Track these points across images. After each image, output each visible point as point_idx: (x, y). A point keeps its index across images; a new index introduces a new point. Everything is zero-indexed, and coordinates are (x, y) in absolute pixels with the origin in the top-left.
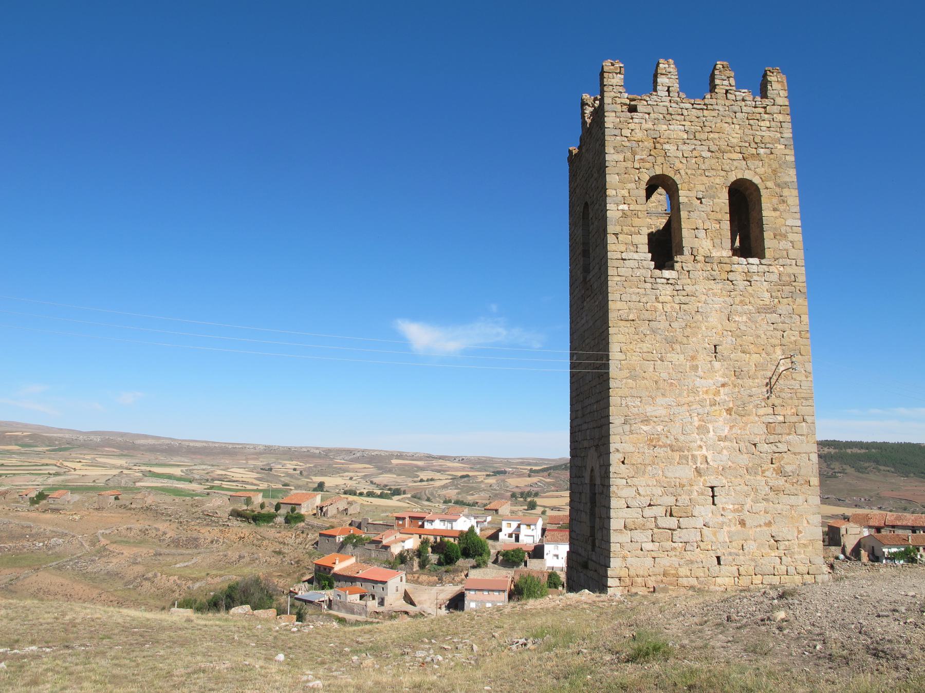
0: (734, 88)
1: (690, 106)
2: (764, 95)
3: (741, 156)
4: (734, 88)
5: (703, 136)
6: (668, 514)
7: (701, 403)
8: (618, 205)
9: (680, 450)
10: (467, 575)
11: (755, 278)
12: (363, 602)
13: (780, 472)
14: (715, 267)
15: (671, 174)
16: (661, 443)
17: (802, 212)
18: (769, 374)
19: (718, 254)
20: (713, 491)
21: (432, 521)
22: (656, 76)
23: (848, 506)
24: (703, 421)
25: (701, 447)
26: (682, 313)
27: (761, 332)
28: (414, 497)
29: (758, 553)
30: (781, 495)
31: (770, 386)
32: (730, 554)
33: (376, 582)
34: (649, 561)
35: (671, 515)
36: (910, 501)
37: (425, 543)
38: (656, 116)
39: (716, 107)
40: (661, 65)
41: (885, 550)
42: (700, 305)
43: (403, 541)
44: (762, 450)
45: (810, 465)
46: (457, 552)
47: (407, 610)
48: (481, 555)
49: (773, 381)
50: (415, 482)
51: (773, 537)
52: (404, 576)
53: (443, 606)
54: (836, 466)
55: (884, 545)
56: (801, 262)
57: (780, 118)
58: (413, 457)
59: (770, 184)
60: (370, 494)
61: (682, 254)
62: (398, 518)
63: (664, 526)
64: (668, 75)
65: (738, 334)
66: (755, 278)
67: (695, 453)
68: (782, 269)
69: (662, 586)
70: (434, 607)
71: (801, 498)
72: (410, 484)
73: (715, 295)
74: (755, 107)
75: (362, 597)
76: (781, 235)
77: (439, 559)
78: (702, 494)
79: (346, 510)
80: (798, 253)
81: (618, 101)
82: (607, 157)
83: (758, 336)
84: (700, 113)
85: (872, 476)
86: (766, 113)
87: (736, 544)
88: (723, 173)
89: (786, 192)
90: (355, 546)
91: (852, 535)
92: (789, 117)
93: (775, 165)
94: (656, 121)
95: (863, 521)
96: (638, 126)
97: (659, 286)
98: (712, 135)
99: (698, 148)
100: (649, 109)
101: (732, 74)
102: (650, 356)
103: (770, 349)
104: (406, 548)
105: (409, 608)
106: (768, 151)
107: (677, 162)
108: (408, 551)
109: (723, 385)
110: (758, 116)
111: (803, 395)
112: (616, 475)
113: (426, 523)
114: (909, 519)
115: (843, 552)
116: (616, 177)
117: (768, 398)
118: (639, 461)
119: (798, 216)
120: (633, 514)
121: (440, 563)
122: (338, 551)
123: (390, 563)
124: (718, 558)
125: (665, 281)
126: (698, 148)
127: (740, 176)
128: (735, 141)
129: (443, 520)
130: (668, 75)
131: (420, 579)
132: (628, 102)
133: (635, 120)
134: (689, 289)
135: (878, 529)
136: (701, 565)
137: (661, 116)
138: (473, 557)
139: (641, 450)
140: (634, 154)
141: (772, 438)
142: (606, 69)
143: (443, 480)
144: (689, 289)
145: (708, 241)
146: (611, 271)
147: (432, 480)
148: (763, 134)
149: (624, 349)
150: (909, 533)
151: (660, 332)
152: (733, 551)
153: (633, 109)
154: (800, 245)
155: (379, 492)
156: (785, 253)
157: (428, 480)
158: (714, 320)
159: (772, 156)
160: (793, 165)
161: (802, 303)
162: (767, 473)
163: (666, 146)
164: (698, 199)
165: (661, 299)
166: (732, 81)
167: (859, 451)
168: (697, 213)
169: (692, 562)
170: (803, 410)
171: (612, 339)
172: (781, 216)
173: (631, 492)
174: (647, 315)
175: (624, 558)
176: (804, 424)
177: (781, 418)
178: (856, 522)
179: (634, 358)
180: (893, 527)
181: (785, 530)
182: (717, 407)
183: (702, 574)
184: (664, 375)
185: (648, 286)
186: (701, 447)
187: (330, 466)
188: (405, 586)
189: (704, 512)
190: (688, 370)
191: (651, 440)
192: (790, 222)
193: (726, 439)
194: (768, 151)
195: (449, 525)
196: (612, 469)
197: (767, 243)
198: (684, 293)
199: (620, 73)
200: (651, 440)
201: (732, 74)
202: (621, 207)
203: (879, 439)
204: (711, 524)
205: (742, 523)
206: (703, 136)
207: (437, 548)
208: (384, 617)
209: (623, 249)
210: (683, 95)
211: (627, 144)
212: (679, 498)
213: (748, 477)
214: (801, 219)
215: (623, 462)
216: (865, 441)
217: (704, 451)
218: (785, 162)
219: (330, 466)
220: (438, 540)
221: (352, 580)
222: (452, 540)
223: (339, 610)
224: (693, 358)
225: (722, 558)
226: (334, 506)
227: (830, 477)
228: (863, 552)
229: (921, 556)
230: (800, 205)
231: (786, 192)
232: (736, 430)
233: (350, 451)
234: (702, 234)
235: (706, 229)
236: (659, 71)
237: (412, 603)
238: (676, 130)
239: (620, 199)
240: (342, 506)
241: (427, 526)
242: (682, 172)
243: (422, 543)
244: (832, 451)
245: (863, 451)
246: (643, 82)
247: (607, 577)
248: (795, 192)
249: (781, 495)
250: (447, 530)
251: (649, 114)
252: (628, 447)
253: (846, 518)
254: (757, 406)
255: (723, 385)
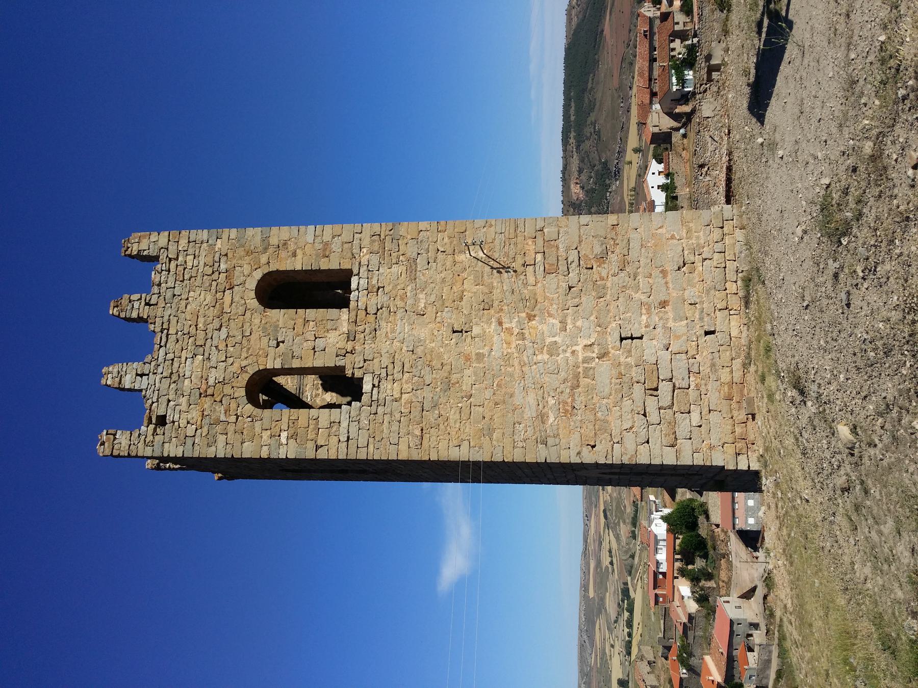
0: (144, 295)
1: (162, 351)
2: (155, 259)
3: (228, 292)
4: (144, 295)
5: (201, 335)
6: (655, 393)
7: (521, 350)
8: (281, 444)
9: (577, 376)
10: (718, 526)
11: (374, 282)
12: (756, 649)
13: (602, 258)
14: (361, 328)
15: (246, 377)
16: (570, 400)
17: (298, 223)
18: (488, 269)
19: (345, 324)
20: (626, 338)
21: (658, 564)
22: (124, 389)
23: (628, 119)
24: (542, 349)
25: (573, 352)
26: (414, 370)
27: (438, 278)
28: (630, 574)
29: (700, 286)
30: (629, 258)
31: (502, 269)
32: (701, 319)
33: (732, 632)
34: (713, 417)
35: (656, 389)
36: (623, 60)
37: (683, 573)
38: (172, 392)
39: (166, 318)
40: (109, 383)
41: (675, 88)
42: (405, 349)
43: (683, 597)
44: (577, 279)
45: (592, 225)
46: (691, 537)
47: (762, 596)
48: (693, 509)
49: (496, 265)
50: (613, 571)
51: (679, 269)
52: (723, 599)
53: (755, 554)
54: (588, 130)
55: (670, 89)
56: (358, 227)
57: (183, 243)
58: (586, 573)
59: (264, 259)
60: (629, 624)
61: (343, 368)
62: (657, 602)
63: (670, 398)
64: (122, 374)
65: (440, 304)
66: (374, 282)
67: (580, 359)
68: (365, 250)
69: (745, 405)
70: (755, 566)
71: (633, 235)
72: (616, 576)
73: (393, 331)
74: (169, 271)
75: (751, 650)
76: (325, 250)
77: (701, 557)
78: (630, 351)
79: (649, 663)
80: (347, 230)
81: (150, 438)
82: (221, 455)
83: (443, 280)
84: (172, 338)
85: (599, 95)
86: (177, 259)
87: (688, 311)
88: (248, 314)
89: (274, 241)
90: (691, 655)
91: (659, 120)
92: (183, 232)
93: (241, 252)
94: (179, 393)
95: (645, 110)
96: (184, 415)
97: (382, 396)
98: (200, 325)
99: (215, 343)
100: (163, 400)
101: (126, 296)
102: (466, 411)
103: (458, 268)
104: (690, 595)
105: (760, 593)
106: (223, 259)
107: (231, 369)
108: (693, 592)
109: (500, 323)
110: (180, 268)
111: (512, 231)
112: (609, 457)
113: (661, 570)
114: (641, 64)
115: (678, 129)
116: (245, 445)
117: (515, 271)
118: (592, 427)
119: (302, 228)
120: (656, 435)
121: (705, 556)
122: (699, 675)
123: (709, 614)
124: (707, 333)
125: (375, 390)
126: (215, 343)
127: (253, 294)
128: (209, 298)
129: (656, 551)
130: (122, 374)
131: (725, 579)
132: (152, 427)
133: (176, 418)
134: (386, 361)
135: (653, 94)
136: (716, 355)
137: (173, 386)
138: (696, 518)
139: (578, 424)
140: (218, 422)
141: (563, 268)
142: (108, 452)
143: (610, 539)
144: (386, 361)
145: (329, 335)
146: (362, 456)
147: (610, 551)
148: (202, 263)
149: (456, 443)
150: (656, 65)
151: (436, 398)
152: (697, 316)
153: (162, 421)
154: (337, 228)
155: (626, 614)
156: (346, 246)
157: (611, 556)
158: (423, 332)
159: (230, 255)
160: (241, 230)
161: (405, 229)
162: (604, 274)
163: (211, 381)
164: (278, 346)
165: (397, 395)
166: (135, 297)
167: (573, 108)
168: (295, 348)
169: (713, 365)
170: (530, 231)
171: (444, 456)
172: (303, 247)
173: (629, 438)
174: (416, 413)
175: (711, 448)
176: (545, 230)
177: (539, 257)
178: (646, 117)
179: (467, 430)
180: (650, 80)
181: (670, 254)
182: (526, 332)
183: (728, 353)
184: (488, 394)
185: (381, 410)
186: (573, 352)
187: (599, 671)
188: (734, 598)
189: (651, 349)
190: (481, 365)
191: (566, 411)
192: (310, 238)
193: (563, 322)
194: (223, 259)
195: (662, 543)
196: (602, 461)
197: (334, 266)
198: (390, 367)
199: (115, 435)
200: (566, 411)
201: (126, 296)
202: (284, 441)
203: (561, 88)
204: (665, 342)
205: (663, 304)
206: (201, 335)
207: (688, 558)
208: (771, 624)
209: (335, 439)
210: (148, 358)
211: (205, 429)
212: (635, 379)
213: (608, 297)
214: (307, 225)
215: (593, 447)
216: (562, 102)
217: (579, 348)
218: (238, 239)
219: (599, 671)
220: (678, 557)
221: (731, 661)
222: (678, 542)
223: (767, 677)
224: (468, 358)
225: (707, 328)
226: (646, 677)
227: (599, 137)
228: (677, 111)
229: (679, 54)
230: (290, 225)
231: (274, 241)
232: (553, 309)
233: (582, 647)
234: (320, 343)
235: (316, 337)
236: (116, 385)
237: (754, 590)
238: (192, 368)
239: (273, 441)
240: (644, 668)
241: (663, 568)
242: (244, 363)
243: (683, 576)
244: (572, 135)
245: (573, 104)
246: (129, 407)
247: (736, 471)
248: (275, 230)
249: (629, 258)
250: (667, 546)
251: (169, 401)
252: (575, 439)
253: (642, 124)
254: (526, 284)
255: (500, 323)
